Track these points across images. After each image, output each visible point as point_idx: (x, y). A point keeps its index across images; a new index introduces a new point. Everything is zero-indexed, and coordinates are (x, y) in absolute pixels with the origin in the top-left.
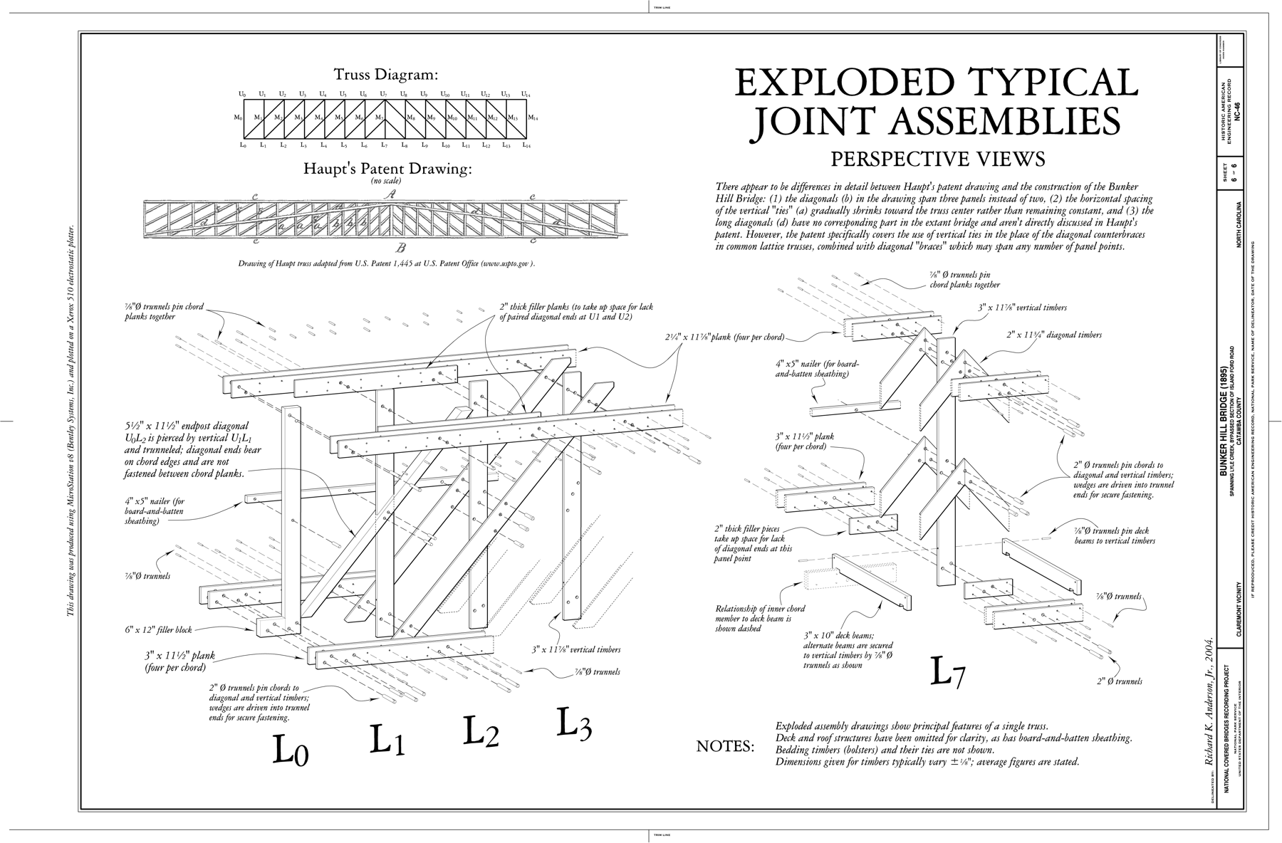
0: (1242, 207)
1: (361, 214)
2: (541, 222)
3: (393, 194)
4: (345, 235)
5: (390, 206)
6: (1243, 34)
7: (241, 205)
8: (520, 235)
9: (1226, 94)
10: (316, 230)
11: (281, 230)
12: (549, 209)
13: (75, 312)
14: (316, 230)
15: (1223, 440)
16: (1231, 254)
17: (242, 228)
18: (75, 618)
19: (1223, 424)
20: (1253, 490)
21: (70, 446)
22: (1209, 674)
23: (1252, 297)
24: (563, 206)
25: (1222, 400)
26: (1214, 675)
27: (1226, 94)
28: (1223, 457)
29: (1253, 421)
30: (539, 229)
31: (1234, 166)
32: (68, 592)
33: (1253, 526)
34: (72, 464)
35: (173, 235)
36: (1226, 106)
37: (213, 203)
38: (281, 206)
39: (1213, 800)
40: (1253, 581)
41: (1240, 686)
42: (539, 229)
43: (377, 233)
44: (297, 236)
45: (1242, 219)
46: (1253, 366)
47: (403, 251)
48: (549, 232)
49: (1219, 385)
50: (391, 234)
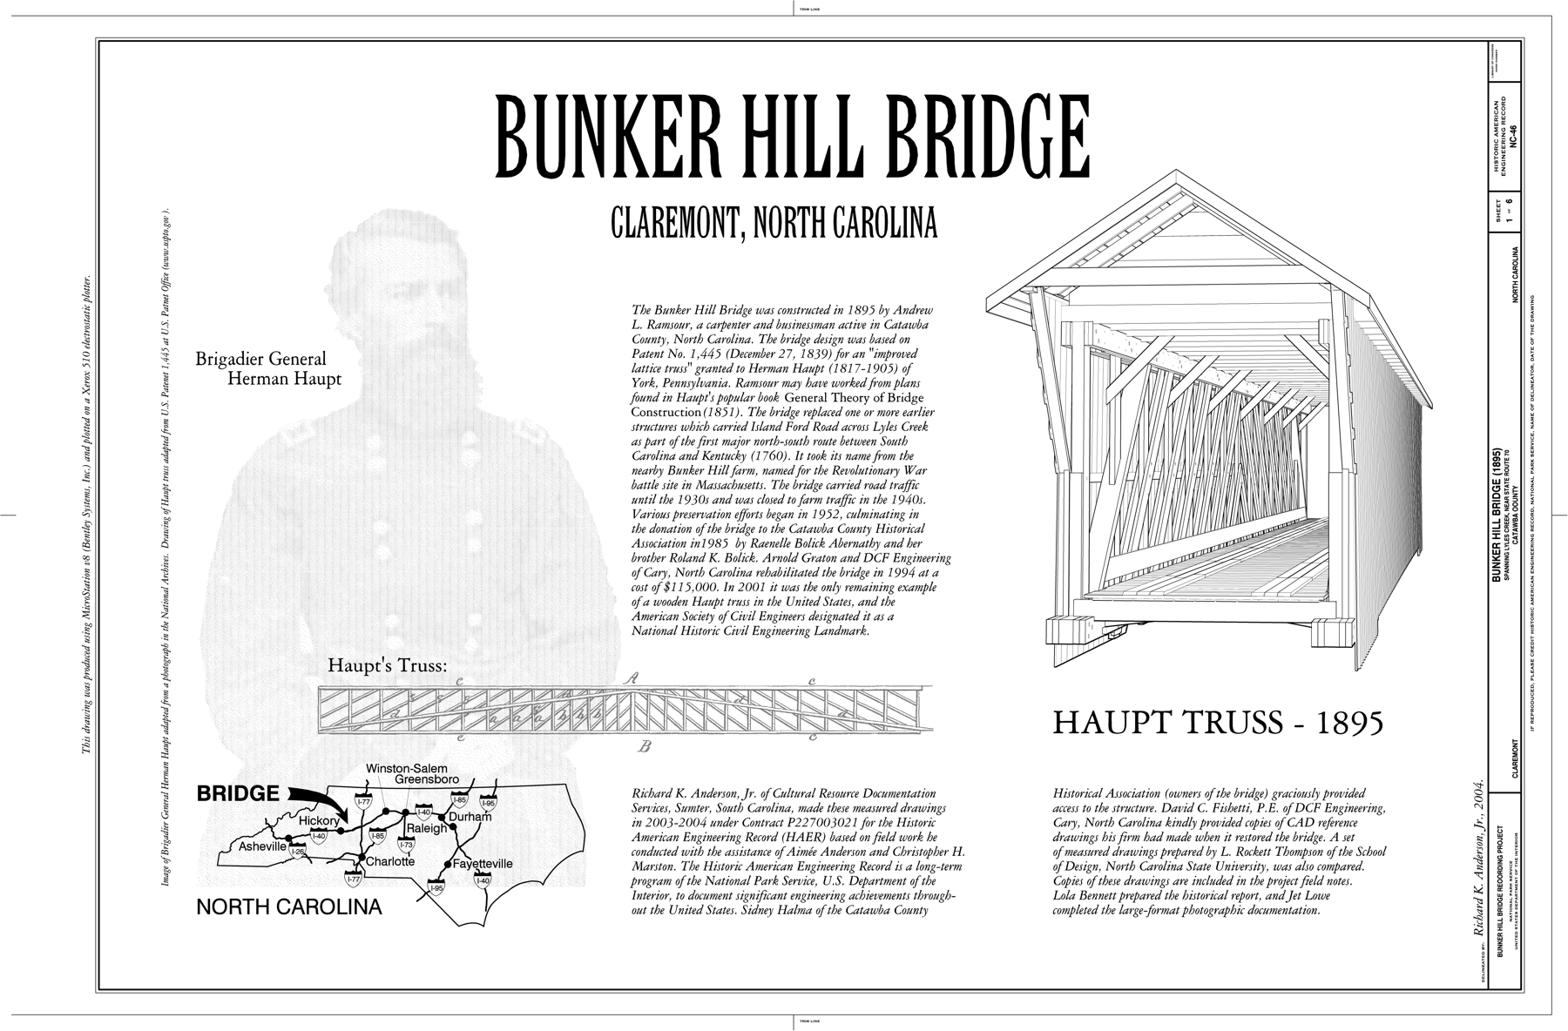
0: (1519, 253)
1: (595, 703)
2: (823, 714)
3: (635, 678)
4: (573, 730)
5: (631, 693)
6: (1521, 41)
7: (441, 692)
8: (797, 730)
9: (1500, 115)
10: (537, 724)
11: (492, 724)
12: (832, 697)
13: (92, 382)
14: (537, 724)
15: (1496, 538)
16: (1506, 311)
17: (443, 721)
18: (92, 755)
19: (1496, 518)
20: (1532, 600)
21: (86, 545)
22: (1478, 825)
23: (1531, 363)
24: (850, 694)
25: (1495, 489)
26: (1485, 825)
27: (1500, 115)
28: (1496, 559)
29: (1532, 515)
30: (820, 722)
31: (1509, 201)
32: (83, 724)
33: (1532, 643)
34: (88, 567)
35: (355, 729)
36: (1499, 130)
37: (406, 690)
38: (493, 693)
39: (1483, 978)
40: (1532, 711)
41: (1516, 838)
42: (820, 722)
43: (614, 727)
44: (513, 731)
45: (1519, 268)
46: (1532, 448)
47: (646, 751)
48: (832, 726)
49: (1491, 471)
50: (633, 728)
